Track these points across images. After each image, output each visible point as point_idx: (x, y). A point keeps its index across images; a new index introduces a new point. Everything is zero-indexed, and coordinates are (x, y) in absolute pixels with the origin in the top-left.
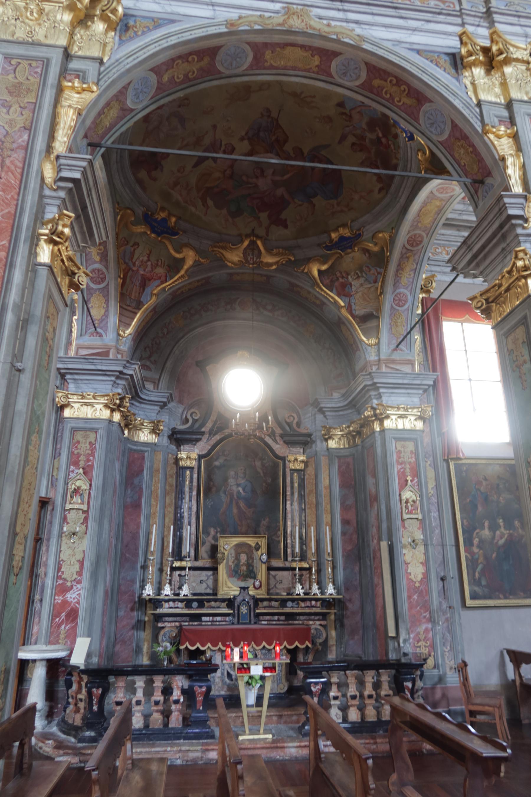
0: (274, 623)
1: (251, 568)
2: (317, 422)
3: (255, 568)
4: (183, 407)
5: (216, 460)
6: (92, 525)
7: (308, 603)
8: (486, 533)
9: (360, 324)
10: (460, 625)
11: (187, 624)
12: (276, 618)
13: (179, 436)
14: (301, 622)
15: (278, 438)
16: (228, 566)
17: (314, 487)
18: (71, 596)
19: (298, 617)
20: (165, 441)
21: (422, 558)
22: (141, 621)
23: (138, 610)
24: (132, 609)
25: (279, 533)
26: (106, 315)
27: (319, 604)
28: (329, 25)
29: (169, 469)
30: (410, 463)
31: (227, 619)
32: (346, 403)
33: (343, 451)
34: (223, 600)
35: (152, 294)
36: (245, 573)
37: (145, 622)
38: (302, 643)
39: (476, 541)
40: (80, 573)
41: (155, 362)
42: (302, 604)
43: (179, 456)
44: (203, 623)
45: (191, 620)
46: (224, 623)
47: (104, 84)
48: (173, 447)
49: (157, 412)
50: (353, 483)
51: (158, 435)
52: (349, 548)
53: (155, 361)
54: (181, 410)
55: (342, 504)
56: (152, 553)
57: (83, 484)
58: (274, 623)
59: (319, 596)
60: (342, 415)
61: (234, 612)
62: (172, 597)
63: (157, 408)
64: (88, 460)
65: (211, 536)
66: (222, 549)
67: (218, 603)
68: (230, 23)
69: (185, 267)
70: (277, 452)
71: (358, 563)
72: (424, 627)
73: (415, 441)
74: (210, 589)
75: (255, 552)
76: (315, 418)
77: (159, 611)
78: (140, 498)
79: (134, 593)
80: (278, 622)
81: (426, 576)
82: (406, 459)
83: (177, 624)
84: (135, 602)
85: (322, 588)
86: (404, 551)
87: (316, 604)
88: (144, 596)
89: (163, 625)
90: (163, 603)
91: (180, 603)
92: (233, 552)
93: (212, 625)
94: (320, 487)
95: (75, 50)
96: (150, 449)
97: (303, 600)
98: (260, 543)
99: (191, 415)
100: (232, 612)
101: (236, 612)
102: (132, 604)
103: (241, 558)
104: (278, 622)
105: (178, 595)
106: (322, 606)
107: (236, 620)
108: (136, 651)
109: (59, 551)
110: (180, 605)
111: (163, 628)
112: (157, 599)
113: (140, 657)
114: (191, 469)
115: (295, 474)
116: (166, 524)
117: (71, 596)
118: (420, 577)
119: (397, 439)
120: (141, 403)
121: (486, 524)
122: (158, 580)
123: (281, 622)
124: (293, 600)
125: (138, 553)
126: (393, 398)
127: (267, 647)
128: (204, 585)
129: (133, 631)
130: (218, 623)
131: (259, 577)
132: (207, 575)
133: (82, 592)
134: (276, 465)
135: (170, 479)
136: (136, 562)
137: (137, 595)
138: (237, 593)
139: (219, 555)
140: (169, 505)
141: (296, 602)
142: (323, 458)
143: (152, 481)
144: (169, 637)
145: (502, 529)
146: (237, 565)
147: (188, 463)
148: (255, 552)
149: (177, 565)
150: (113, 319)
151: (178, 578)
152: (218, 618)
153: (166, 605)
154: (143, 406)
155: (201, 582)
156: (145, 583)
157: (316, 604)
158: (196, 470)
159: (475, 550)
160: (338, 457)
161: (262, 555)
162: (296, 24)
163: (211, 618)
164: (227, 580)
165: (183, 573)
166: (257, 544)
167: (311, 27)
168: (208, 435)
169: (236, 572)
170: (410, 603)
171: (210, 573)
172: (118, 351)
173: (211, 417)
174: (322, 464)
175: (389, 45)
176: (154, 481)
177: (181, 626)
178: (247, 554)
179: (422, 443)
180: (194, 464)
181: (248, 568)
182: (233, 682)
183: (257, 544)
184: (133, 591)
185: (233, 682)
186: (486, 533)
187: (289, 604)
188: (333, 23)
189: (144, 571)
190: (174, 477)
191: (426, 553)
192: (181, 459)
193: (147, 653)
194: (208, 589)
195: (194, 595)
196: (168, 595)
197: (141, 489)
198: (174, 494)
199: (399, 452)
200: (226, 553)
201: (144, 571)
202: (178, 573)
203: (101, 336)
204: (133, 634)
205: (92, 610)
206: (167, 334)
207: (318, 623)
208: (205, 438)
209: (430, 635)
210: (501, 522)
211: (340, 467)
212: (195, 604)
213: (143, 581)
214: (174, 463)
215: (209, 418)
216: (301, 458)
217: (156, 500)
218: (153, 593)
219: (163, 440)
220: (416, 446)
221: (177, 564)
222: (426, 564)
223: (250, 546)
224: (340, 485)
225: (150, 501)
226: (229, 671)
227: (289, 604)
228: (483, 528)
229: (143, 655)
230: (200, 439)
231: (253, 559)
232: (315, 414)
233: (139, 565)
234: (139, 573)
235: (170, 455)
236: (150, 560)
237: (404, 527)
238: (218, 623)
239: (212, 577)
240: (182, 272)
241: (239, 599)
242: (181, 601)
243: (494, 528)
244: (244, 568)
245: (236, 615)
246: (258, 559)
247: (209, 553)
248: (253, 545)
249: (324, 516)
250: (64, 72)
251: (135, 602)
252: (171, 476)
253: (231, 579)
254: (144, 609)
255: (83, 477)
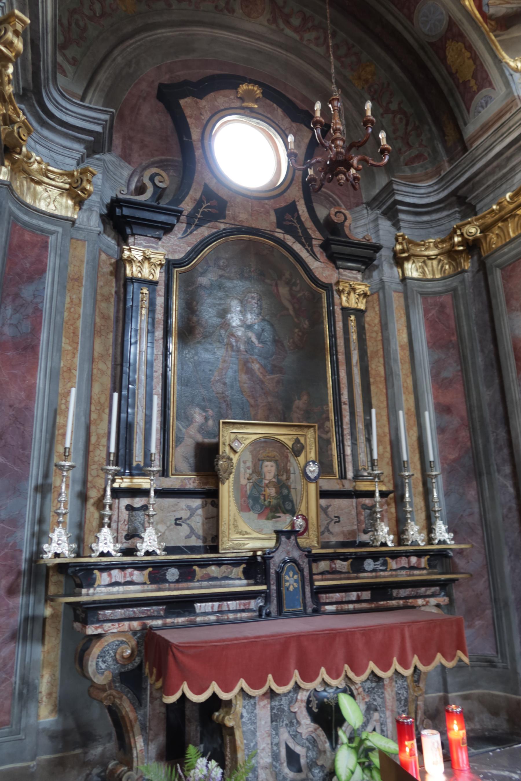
0: (351, 606)
1: (285, 492)
2: (381, 233)
3: (293, 491)
4: (132, 168)
5: (202, 274)
7: (403, 562)
9: (498, 32)
11: (160, 622)
12: (353, 595)
13: (126, 211)
14: (401, 602)
15: (317, 250)
16: (238, 487)
17: (380, 346)
19: (395, 592)
22: (34, 618)
23: (28, 592)
24: (11, 591)
25: (327, 424)
27: (424, 561)
29: (101, 283)
31: (253, 604)
32: (442, 195)
33: (429, 284)
34: (235, 563)
36: (274, 502)
37: (45, 619)
38: (449, 657)
41: (74, 62)
42: (393, 564)
43: (126, 254)
44: (199, 619)
45: (168, 614)
46: (245, 615)
48: (110, 241)
49: (78, 156)
50: (454, 339)
51: (79, 202)
52: (452, 457)
53: (74, 58)
54: (126, 173)
55: (435, 376)
56: (66, 455)
58: (351, 606)
59: (422, 545)
60: (427, 222)
61: (269, 588)
62: (118, 558)
63: (80, 148)
65: (196, 425)
66: (227, 449)
67: (223, 568)
70: (317, 274)
71: (474, 483)
74: (198, 537)
75: (292, 458)
76: (377, 225)
78: (36, 330)
79: (17, 550)
80: (358, 606)
83: (136, 625)
84: (19, 573)
87: (419, 562)
88: (48, 557)
89: (100, 631)
90: (96, 572)
91: (136, 572)
92: (248, 457)
93: (219, 623)
94: (392, 346)
96: (60, 230)
97: (395, 555)
98: (302, 440)
99: (152, 179)
100: (264, 587)
101: (274, 587)
102: (11, 578)
103: (265, 469)
104: (358, 606)
105: (130, 552)
106: (431, 565)
107: (273, 608)
108: (21, 694)
110: (137, 576)
111: (99, 636)
112: (80, 565)
113: (32, 707)
114: (152, 284)
115: (353, 317)
116: (95, 397)
120: (43, 124)
122: (77, 519)
123: (364, 605)
124: (375, 556)
125: (28, 457)
127: (379, 673)
128: (184, 530)
129: (12, 645)
130: (231, 616)
131: (303, 509)
132: (189, 508)
134: (316, 299)
135: (104, 305)
136: (25, 476)
137: (25, 555)
138: (272, 543)
139: (221, 462)
140: (102, 356)
141: (381, 560)
142: (395, 295)
143: (64, 296)
144: (115, 660)
146: (257, 486)
147: (146, 272)
148: (292, 458)
149: (123, 485)
151: (125, 515)
152: (233, 605)
153: (104, 578)
154: (46, 133)
155: (178, 522)
156: (45, 527)
157: (419, 562)
158: (161, 289)
160: (422, 294)
161: (307, 464)
163: (216, 604)
164: (238, 517)
165: (138, 502)
166: (297, 441)
168: (185, 225)
169: (256, 500)
171: (197, 502)
173: (191, 192)
174: (395, 306)
176: (68, 300)
177: (144, 627)
178: (276, 461)
180: (158, 275)
181: (279, 492)
182: (302, 776)
183: (297, 441)
184: (15, 544)
185: (302, 776)
187: (369, 565)
189: (43, 498)
190: (112, 300)
192: (130, 261)
193: (50, 694)
194: (194, 538)
195: (169, 550)
196: (108, 554)
197: (38, 311)
198: (111, 336)
200: (235, 458)
201: (43, 498)
202: (125, 502)
204: (13, 653)
206: (101, 16)
207: (433, 601)
208: (180, 228)
211: (426, 311)
212: (173, 574)
213: (41, 521)
214: (111, 273)
215: (187, 194)
216: (362, 288)
217: (74, 343)
218: (71, 551)
219: (89, 219)
221: (123, 483)
223: (283, 445)
224: (428, 343)
225: (60, 341)
226: (292, 745)
227: (369, 565)
229: (38, 702)
230: (168, 229)
231: (288, 472)
232: (376, 220)
233: (32, 483)
234: (29, 503)
235: (103, 256)
236: (61, 468)
238: (231, 616)
239: (200, 512)
241: (278, 558)
242: (140, 567)
244: (272, 491)
245: (274, 595)
246: (298, 472)
247: (192, 460)
248: (290, 444)
249: (404, 398)
251: (19, 573)
252: (107, 299)
253: (246, 514)
254: (42, 588)
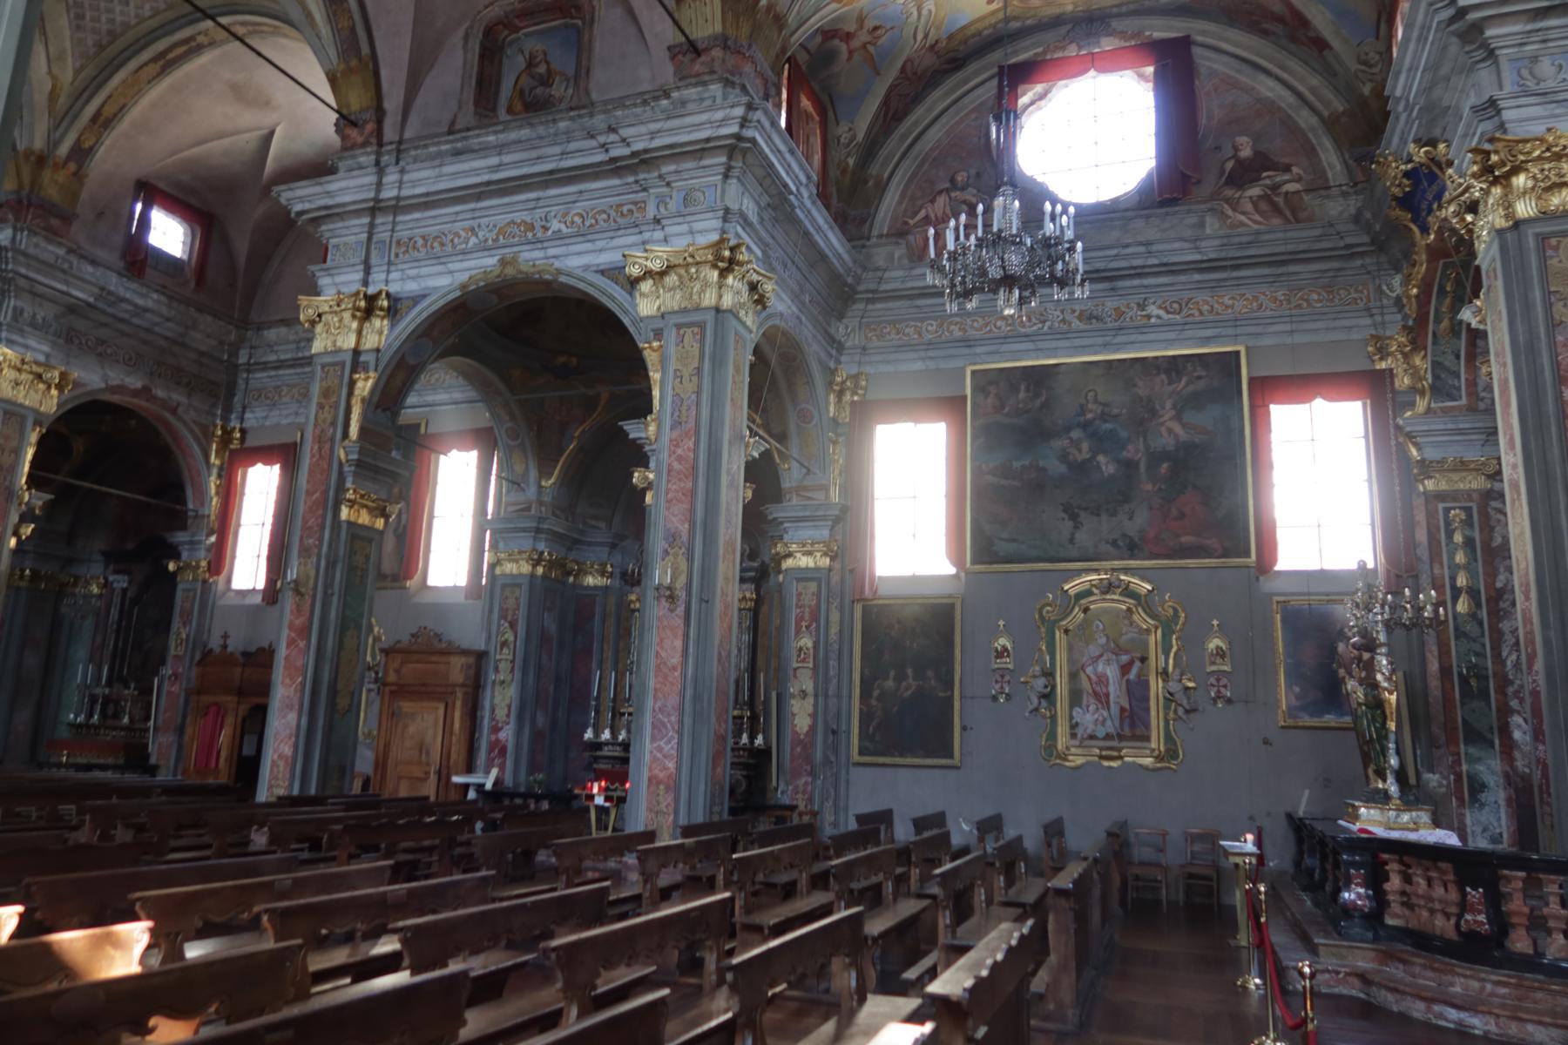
6: (517, 674)
8: (890, 684)
10: (848, 782)
18: (502, 735)
20: (617, 583)
21: (810, 709)
26: (527, 470)
28: (534, 265)
30: (810, 606)
35: (573, 438)
39: (876, 693)
40: (508, 716)
47: (380, 369)
57: (510, 636)
64: (514, 615)
68: (463, 286)
69: (602, 403)
72: (804, 780)
73: (819, 580)
77: (599, 753)
81: (813, 728)
82: (807, 602)
85: (752, 738)
86: (793, 702)
95: (362, 348)
109: (493, 697)
117: (502, 735)
118: (806, 729)
119: (799, 580)
121: (892, 674)
126: (800, 532)
133: (510, 733)
145: (911, 680)
150: (533, 474)
159: (874, 702)
162: (510, 271)
167: (521, 272)
170: (792, 755)
172: (541, 503)
175: (579, 272)
179: (828, 584)
186: (890, 684)
188: (537, 263)
191: (816, 705)
199: (799, 595)
203: (524, 490)
205: (518, 747)
209: (809, 788)
210: (910, 672)
220: (819, 587)
222: (814, 716)
228: (886, 678)
237: (795, 676)
240: (599, 409)
243: (901, 676)
250: (354, 370)
255: (509, 630)
